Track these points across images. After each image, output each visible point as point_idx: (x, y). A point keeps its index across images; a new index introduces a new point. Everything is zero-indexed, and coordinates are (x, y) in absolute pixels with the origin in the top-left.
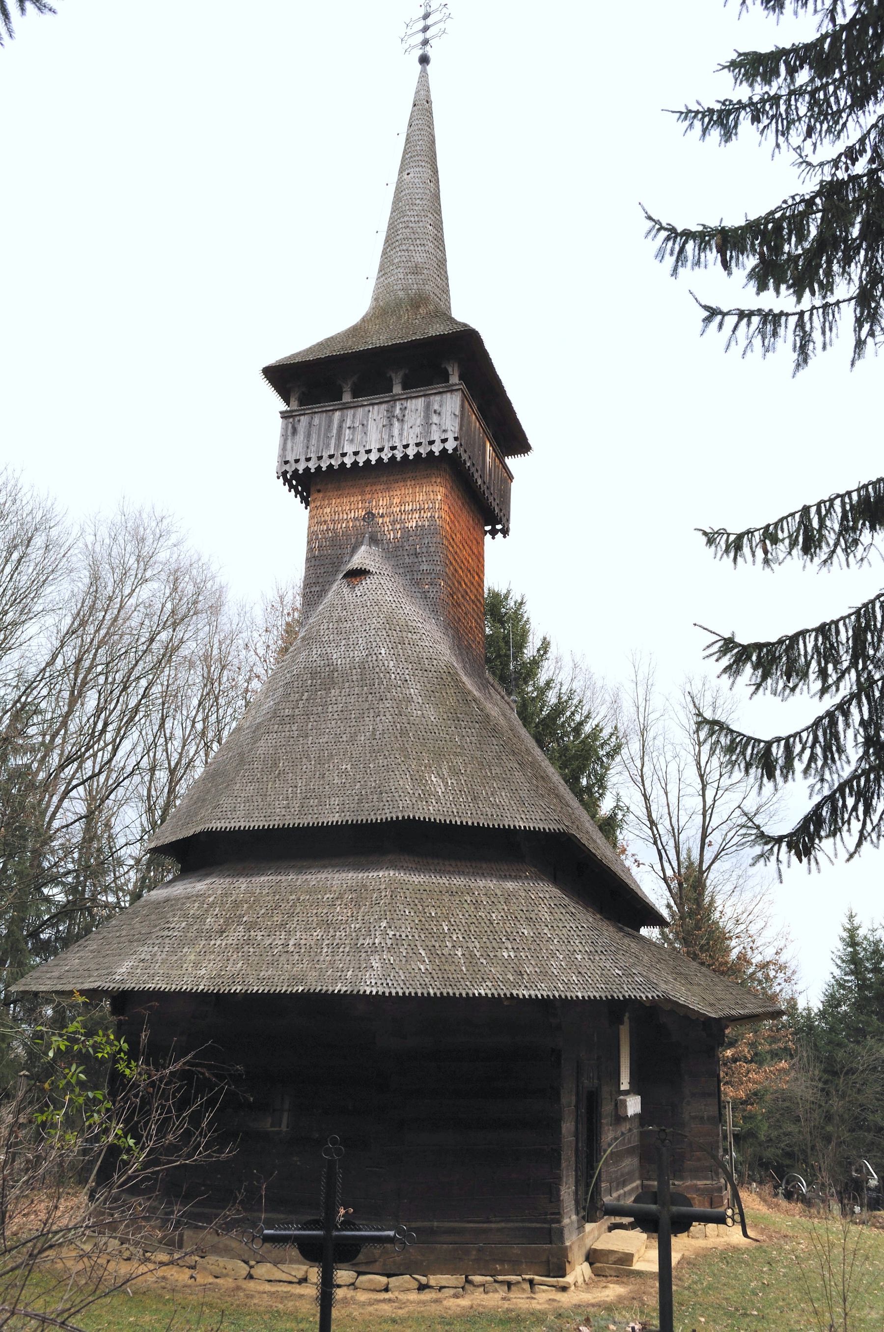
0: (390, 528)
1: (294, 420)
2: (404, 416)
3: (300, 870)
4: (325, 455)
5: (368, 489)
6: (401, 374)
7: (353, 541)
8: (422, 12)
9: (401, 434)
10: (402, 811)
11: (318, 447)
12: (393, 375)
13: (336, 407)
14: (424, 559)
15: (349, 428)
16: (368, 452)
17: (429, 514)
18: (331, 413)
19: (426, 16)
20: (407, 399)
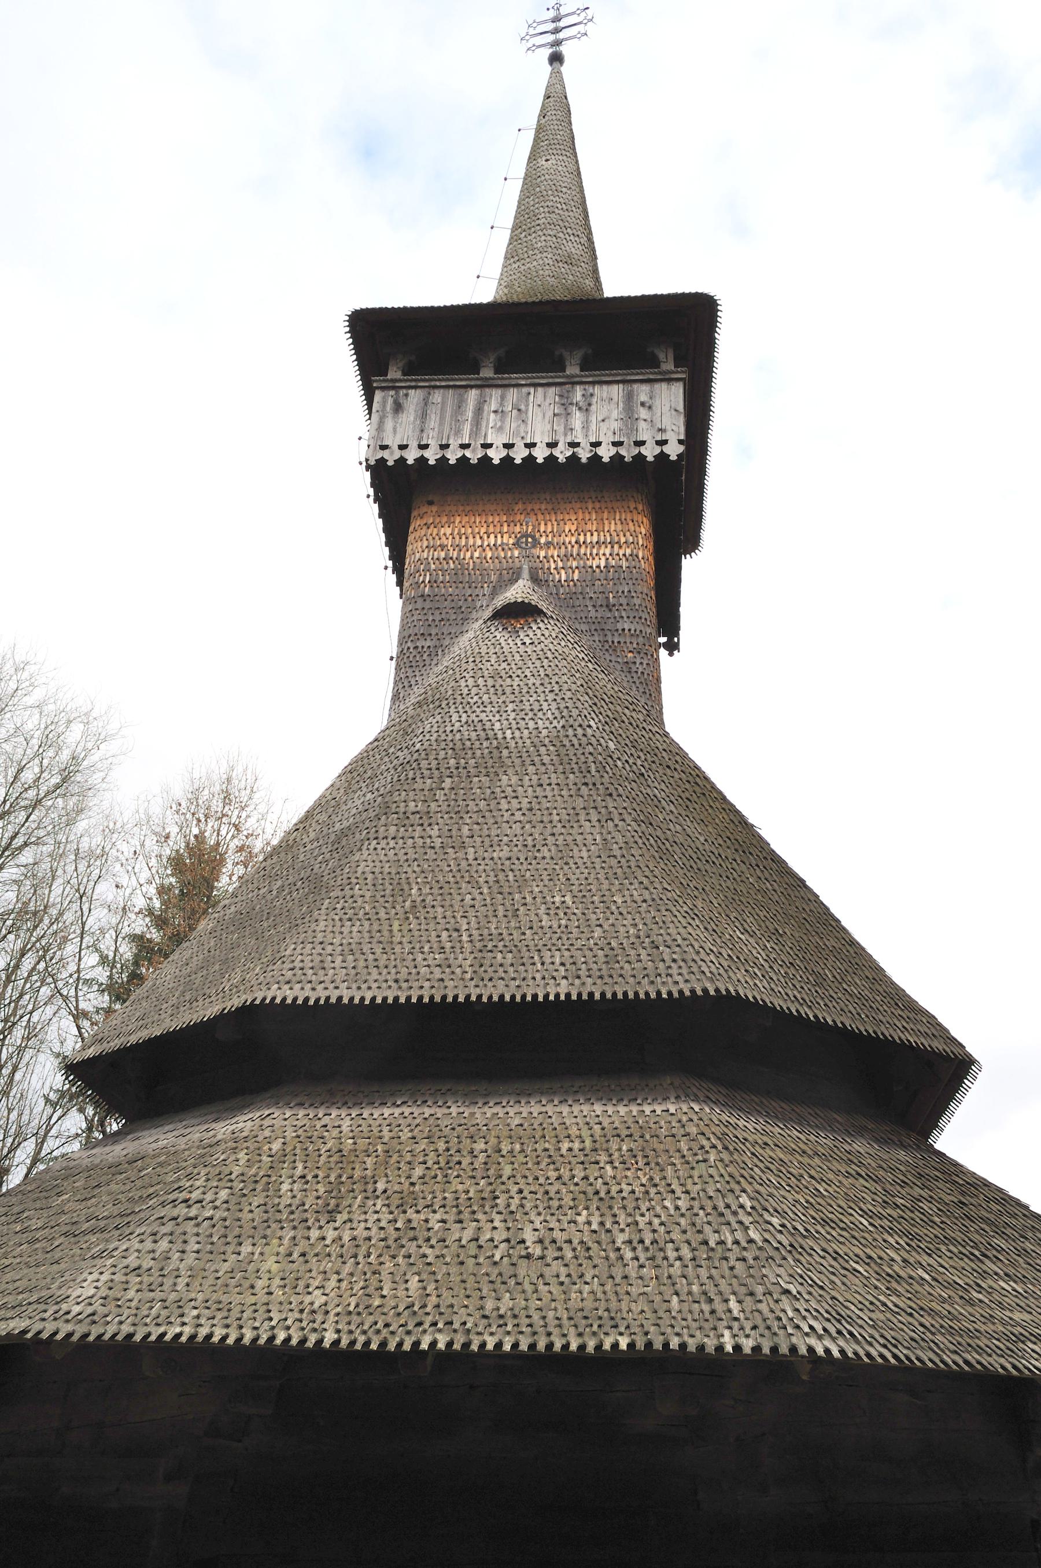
0: (560, 564)
1: (397, 393)
2: (590, 405)
3: (471, 1098)
4: (454, 443)
5: (520, 506)
6: (578, 355)
7: (493, 578)
8: (552, 14)
9: (586, 427)
10: (711, 980)
11: (441, 432)
12: (566, 354)
13: (472, 383)
14: (624, 614)
15: (495, 412)
16: (531, 446)
17: (628, 552)
18: (462, 391)
19: (557, 19)
20: (593, 383)
